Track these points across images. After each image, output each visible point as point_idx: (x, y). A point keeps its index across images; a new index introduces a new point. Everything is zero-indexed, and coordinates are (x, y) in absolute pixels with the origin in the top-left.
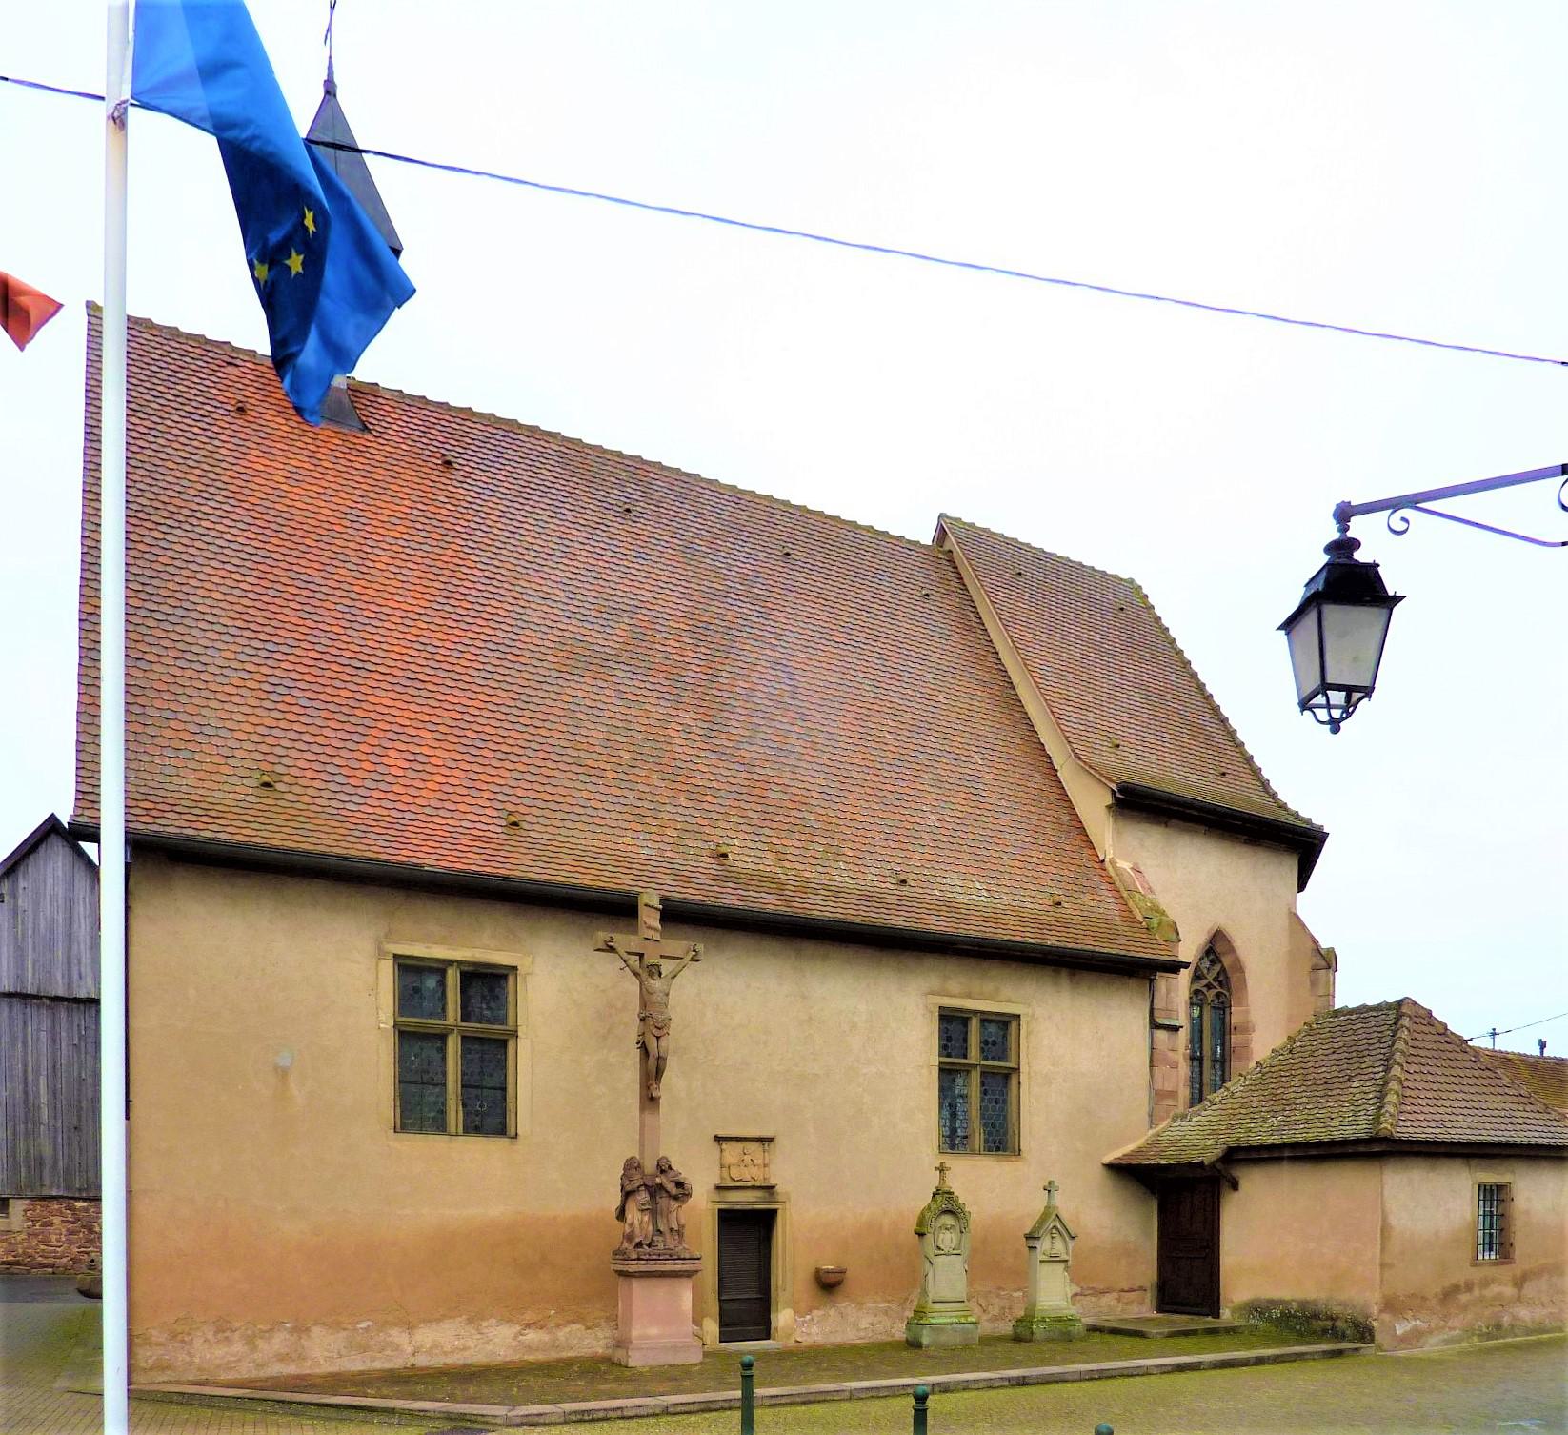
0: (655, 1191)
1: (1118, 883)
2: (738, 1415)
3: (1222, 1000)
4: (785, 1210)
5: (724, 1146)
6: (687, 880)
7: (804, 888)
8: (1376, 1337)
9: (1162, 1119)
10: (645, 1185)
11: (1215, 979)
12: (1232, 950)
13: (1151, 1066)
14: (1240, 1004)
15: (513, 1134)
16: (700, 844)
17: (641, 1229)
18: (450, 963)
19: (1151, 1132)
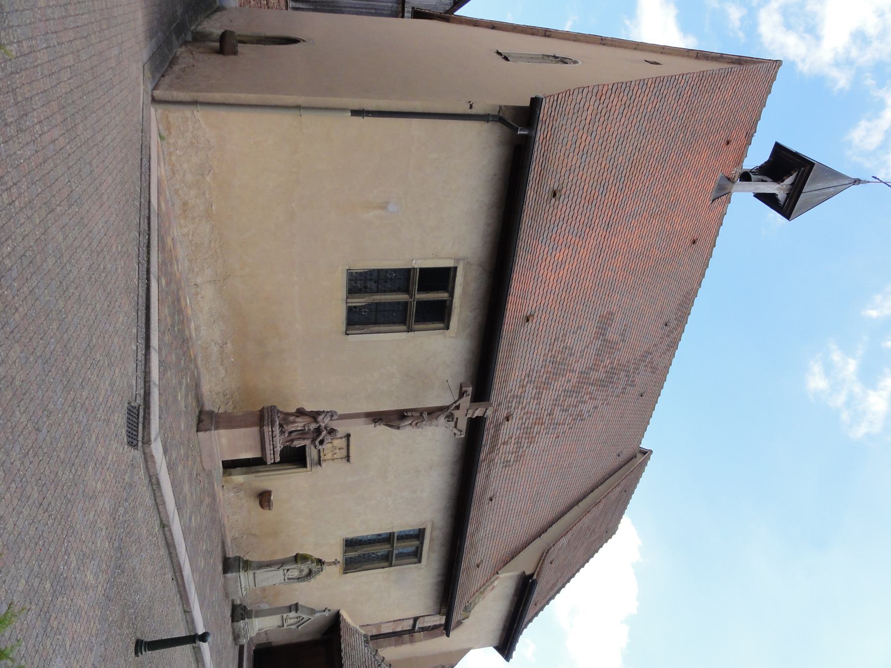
1: (487, 584)
4: (307, 471)
13: (394, 621)
14: (424, 636)
15: (348, 332)
18: (452, 295)
19: (358, 627)
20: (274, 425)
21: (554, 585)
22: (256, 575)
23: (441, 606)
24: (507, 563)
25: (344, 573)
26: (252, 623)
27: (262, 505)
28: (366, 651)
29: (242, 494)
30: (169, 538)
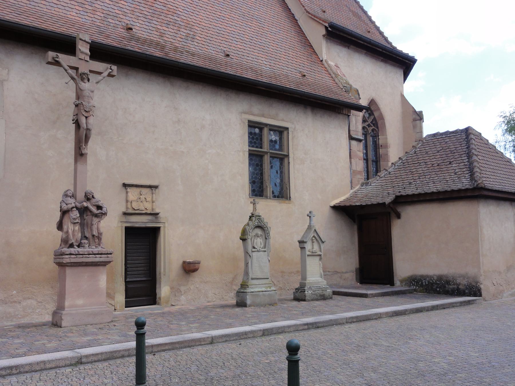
0: (83, 211)
1: (330, 71)
2: (134, 359)
3: (375, 132)
6: (108, 36)
7: (176, 49)
8: (483, 293)
9: (357, 185)
10: (76, 207)
11: (371, 122)
12: (378, 109)
13: (350, 158)
16: (117, 22)
17: (74, 235)
19: (352, 191)
20: (63, 253)
21: (355, 14)
22: (254, 277)
23: (339, 113)
24: (315, 52)
25: (290, 200)
26: (310, 283)
27: (195, 270)
28: (375, 184)
29: (183, 289)
30: (104, 357)
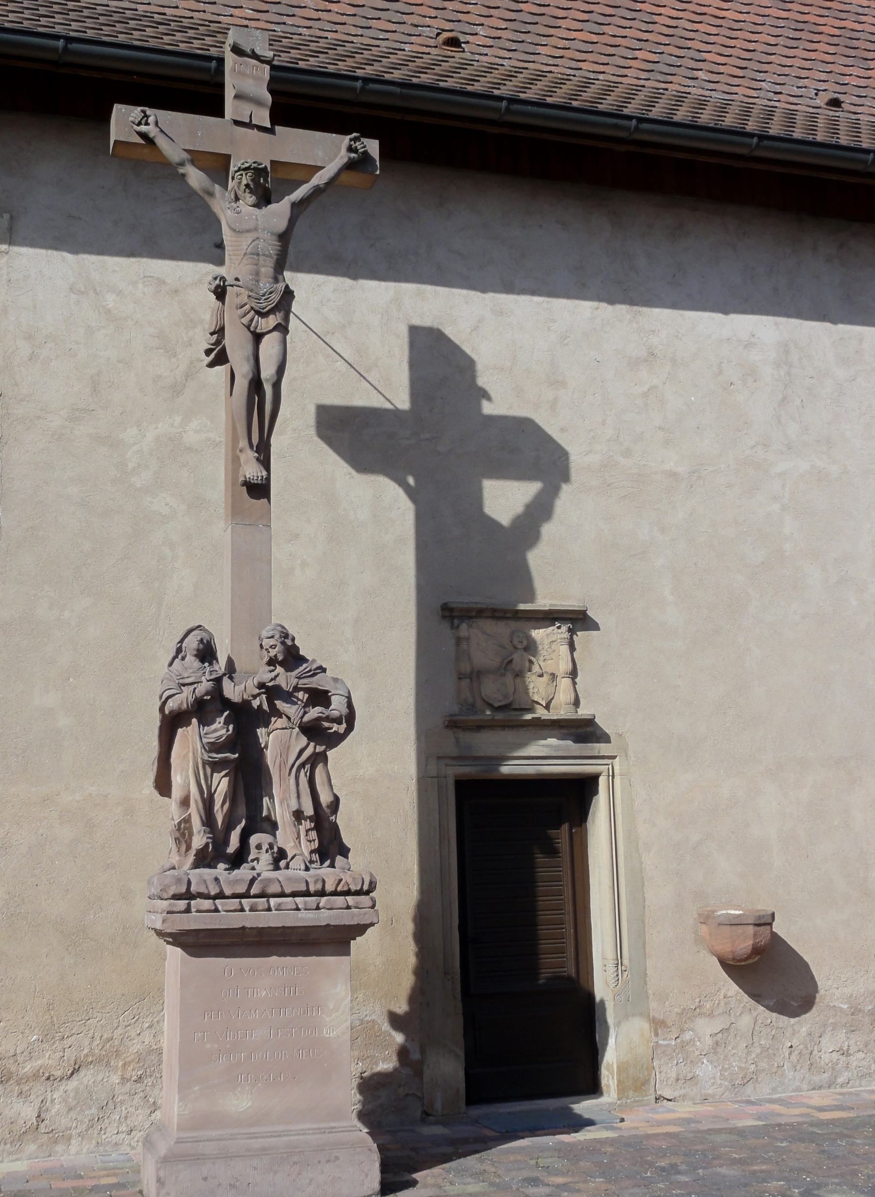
5: (464, 630)
